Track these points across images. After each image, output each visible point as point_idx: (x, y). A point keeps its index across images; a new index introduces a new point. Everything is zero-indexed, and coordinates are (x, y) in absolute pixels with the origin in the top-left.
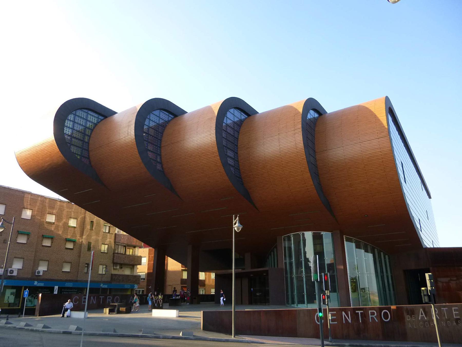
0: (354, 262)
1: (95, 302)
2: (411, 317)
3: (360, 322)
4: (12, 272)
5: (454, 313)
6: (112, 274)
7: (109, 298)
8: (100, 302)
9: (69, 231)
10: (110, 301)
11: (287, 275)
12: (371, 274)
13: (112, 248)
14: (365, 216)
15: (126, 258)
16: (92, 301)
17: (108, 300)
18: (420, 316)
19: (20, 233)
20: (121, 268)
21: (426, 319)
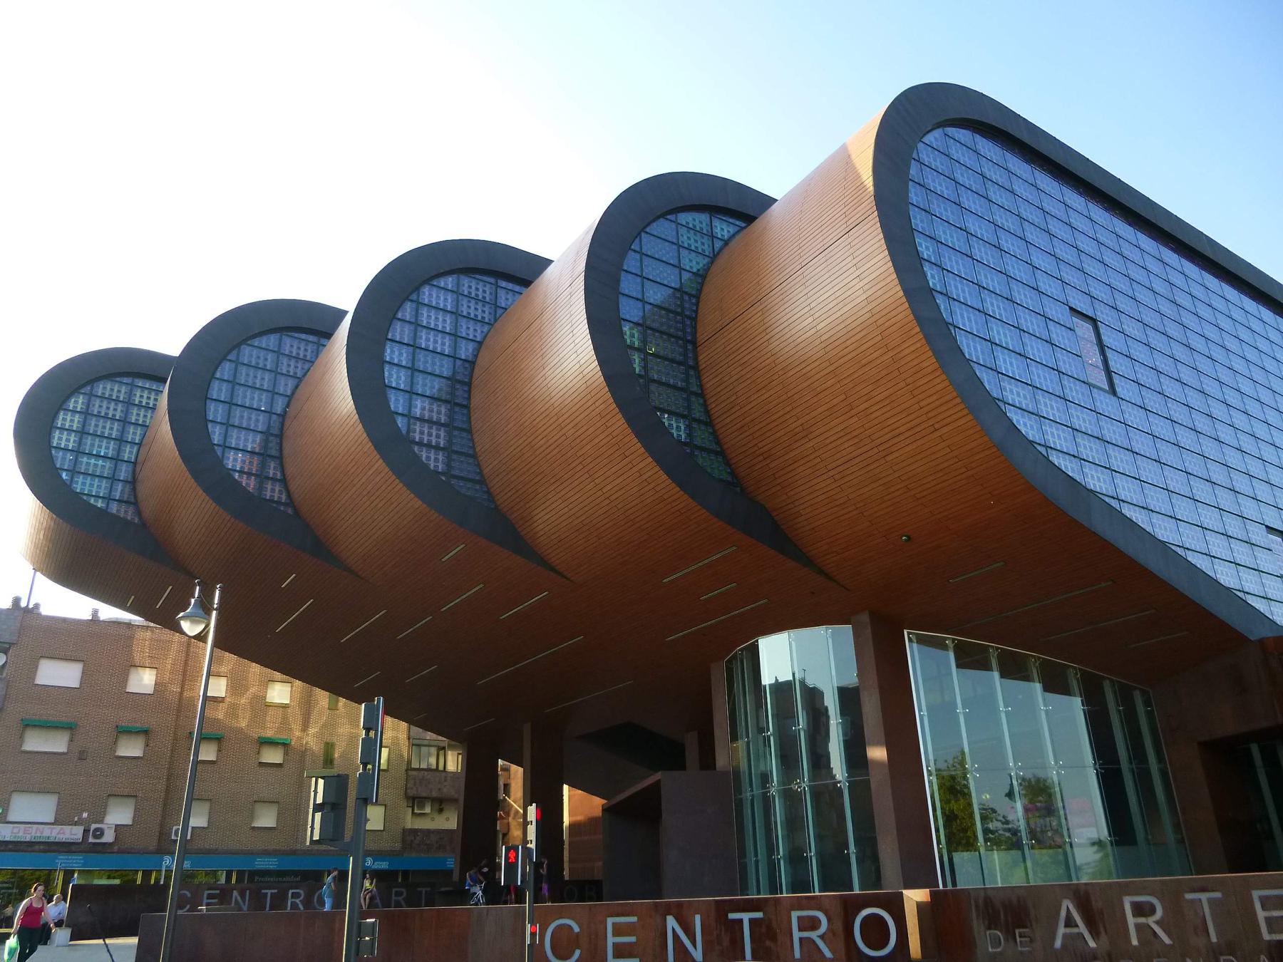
2: (1010, 935)
4: (99, 833)
5: (1261, 915)
6: (404, 830)
7: (295, 895)
9: (268, 718)
10: (299, 903)
12: (1085, 767)
13: (402, 756)
14: (901, 538)
15: (445, 781)
18: (1061, 930)
19: (124, 732)
20: (441, 811)
21: (1092, 944)
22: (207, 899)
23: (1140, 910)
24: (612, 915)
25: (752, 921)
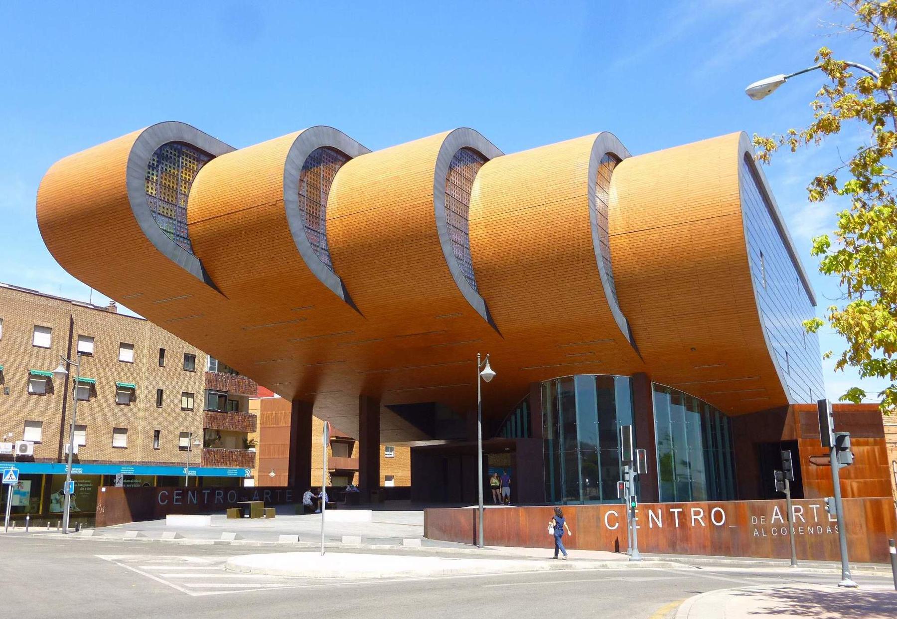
3: (677, 526)
4: (24, 448)
5: (175, 497)
8: (204, 502)
11: (548, 451)
16: (191, 499)
17: (216, 497)
18: (774, 517)
23: (797, 510)
24: (794, 505)
25: (678, 512)
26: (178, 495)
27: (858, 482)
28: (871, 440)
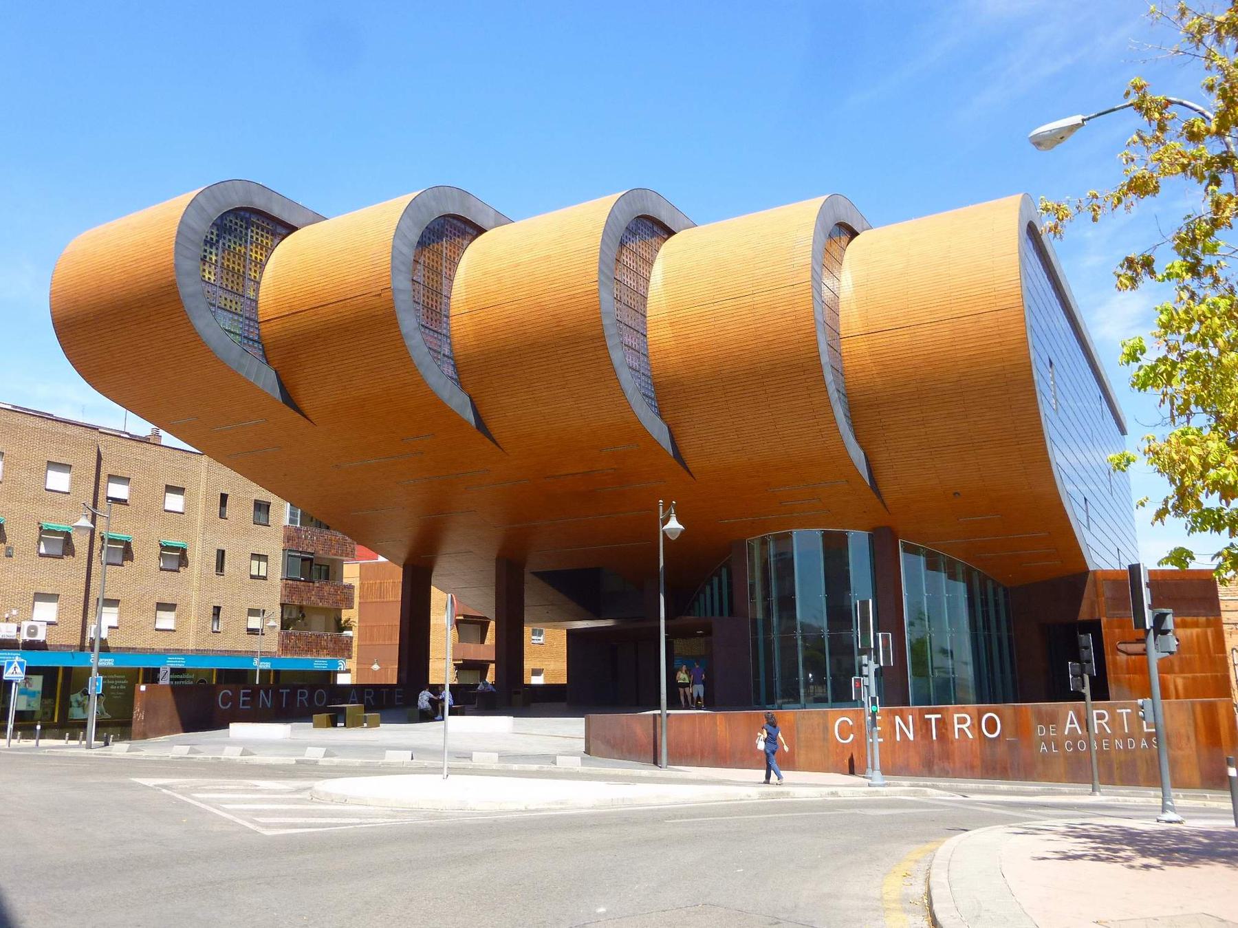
0: (921, 602)
1: (269, 705)
3: (934, 738)
4: (33, 631)
5: (242, 699)
17: (299, 698)
18: (1068, 725)
22: (243, 697)
25: (936, 719)
26: (245, 695)
27: (1184, 678)
28: (1202, 619)
